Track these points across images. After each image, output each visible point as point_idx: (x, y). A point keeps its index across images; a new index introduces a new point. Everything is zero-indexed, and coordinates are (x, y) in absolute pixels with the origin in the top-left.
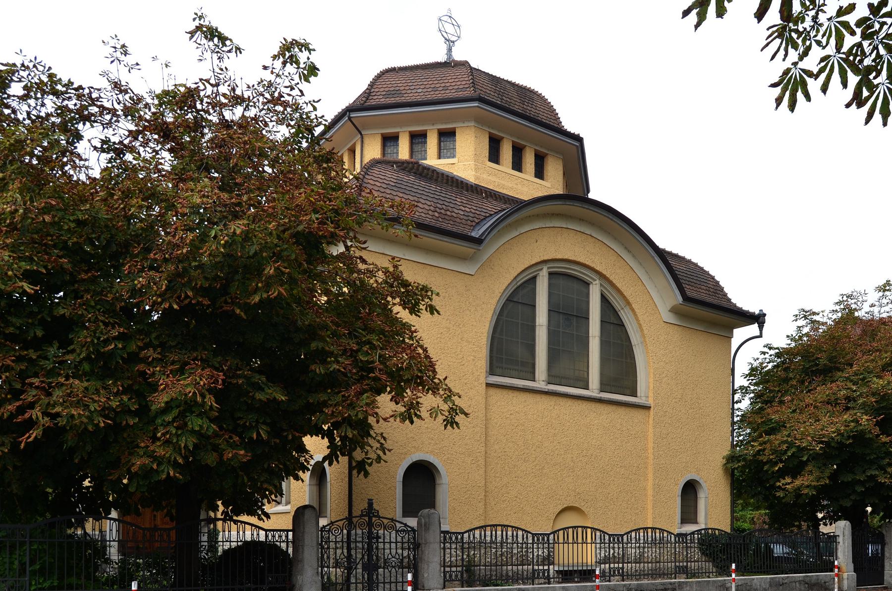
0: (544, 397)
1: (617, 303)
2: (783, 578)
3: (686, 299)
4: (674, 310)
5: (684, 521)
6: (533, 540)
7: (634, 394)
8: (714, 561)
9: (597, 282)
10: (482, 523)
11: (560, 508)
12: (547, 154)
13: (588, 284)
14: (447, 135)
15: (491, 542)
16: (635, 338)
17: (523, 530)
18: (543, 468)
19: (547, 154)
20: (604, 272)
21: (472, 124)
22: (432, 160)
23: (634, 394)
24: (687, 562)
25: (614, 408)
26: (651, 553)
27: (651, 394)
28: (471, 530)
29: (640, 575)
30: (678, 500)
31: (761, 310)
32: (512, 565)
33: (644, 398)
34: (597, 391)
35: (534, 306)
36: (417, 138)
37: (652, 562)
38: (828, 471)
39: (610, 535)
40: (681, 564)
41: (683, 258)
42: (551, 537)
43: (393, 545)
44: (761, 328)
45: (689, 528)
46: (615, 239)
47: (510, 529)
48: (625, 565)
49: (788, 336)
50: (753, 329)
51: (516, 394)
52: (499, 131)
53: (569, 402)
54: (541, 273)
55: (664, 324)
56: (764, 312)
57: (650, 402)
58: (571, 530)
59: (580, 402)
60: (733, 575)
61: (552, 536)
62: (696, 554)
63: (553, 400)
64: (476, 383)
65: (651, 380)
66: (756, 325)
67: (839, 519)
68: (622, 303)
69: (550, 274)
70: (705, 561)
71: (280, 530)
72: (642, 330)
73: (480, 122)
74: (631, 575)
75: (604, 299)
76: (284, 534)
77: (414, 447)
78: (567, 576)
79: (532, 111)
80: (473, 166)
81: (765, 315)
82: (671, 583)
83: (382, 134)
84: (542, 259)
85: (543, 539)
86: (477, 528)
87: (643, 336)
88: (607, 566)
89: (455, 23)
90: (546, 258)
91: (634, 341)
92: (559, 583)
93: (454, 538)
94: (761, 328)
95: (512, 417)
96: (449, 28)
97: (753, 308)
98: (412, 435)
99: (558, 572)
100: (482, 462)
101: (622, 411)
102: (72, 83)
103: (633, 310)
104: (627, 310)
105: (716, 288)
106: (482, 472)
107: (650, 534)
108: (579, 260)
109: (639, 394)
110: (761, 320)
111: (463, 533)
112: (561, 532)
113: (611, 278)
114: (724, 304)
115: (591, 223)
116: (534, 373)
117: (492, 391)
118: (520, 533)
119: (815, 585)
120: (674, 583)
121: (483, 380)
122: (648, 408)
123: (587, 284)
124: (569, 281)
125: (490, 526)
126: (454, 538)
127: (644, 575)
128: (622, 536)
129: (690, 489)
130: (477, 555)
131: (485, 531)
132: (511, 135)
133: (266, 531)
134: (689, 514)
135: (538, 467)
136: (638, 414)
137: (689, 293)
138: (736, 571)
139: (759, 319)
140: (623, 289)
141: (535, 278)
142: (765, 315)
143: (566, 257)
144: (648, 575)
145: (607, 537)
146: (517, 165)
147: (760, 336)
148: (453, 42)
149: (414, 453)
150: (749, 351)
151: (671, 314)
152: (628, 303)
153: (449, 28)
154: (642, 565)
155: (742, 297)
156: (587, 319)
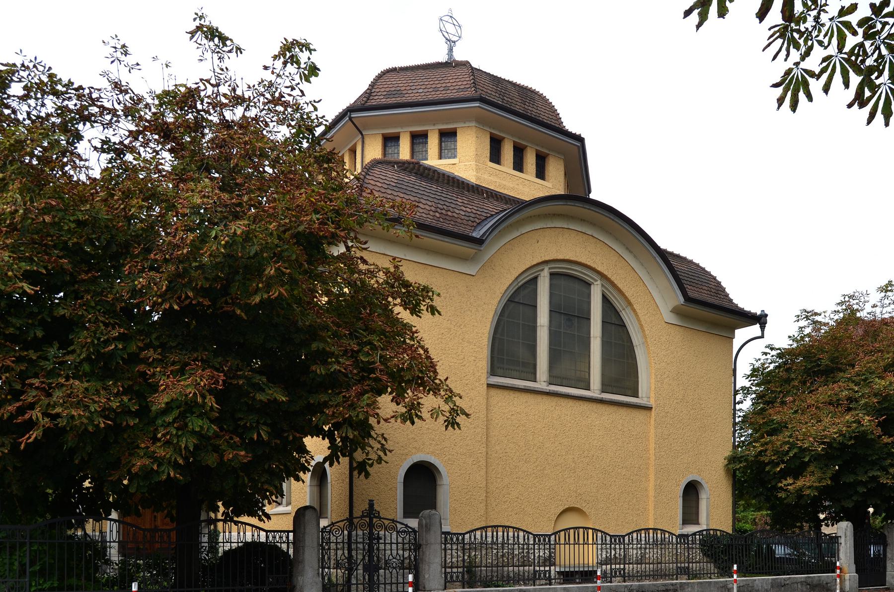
0: (545, 398)
1: (618, 304)
3: (688, 299)
4: (676, 311)
5: (686, 521)
6: (534, 540)
7: (636, 395)
9: (599, 282)
10: (483, 524)
11: (562, 509)
15: (493, 543)
16: (636, 339)
17: (524, 531)
18: (544, 469)
20: (606, 273)
21: (474, 124)
22: (433, 160)
23: (636, 395)
24: (689, 563)
26: (652, 554)
27: (652, 395)
28: (472, 531)
29: (641, 576)
30: (680, 501)
31: (763, 311)
32: (513, 566)
33: (645, 399)
34: (598, 392)
35: (535, 307)
36: (418, 138)
37: (653, 563)
39: (611, 536)
40: (683, 565)
41: (685, 259)
42: (553, 537)
43: (394, 546)
44: (763, 328)
45: (691, 529)
46: (617, 239)
47: (511, 530)
48: (627, 566)
49: (790, 337)
50: (755, 330)
51: (517, 394)
52: (500, 131)
53: (571, 403)
54: (542, 274)
55: (665, 325)
56: (766, 312)
57: (652, 403)
58: (572, 531)
59: (581, 403)
60: (735, 576)
61: (553, 537)
62: (698, 555)
63: (554, 401)
64: (477, 384)
65: (653, 381)
66: (758, 325)
67: (841, 520)
69: (551, 274)
70: (707, 562)
71: (281, 531)
72: (643, 331)
73: (481, 122)
74: (633, 576)
75: (605, 299)
76: (284, 535)
77: (415, 448)
78: (568, 576)
79: (533, 111)
80: (474, 167)
81: (766, 315)
84: (544, 259)
85: (544, 540)
86: (478, 529)
87: (645, 336)
88: (609, 566)
89: (455, 23)
90: (547, 258)
91: (635, 341)
92: (560, 584)
93: (455, 539)
94: (763, 328)
95: (513, 417)
96: (450, 29)
97: (754, 308)
98: (413, 436)
99: (559, 573)
100: (483, 462)
101: (623, 411)
102: (73, 84)
103: (634, 311)
104: (628, 310)
105: (718, 289)
107: (651, 535)
108: (580, 260)
109: (640, 395)
110: (762, 320)
111: (464, 534)
112: (562, 533)
113: (613, 279)
114: (726, 304)
115: (593, 224)
116: (535, 374)
117: (493, 392)
118: (521, 534)
119: (816, 586)
120: (676, 584)
121: (484, 381)
122: (649, 409)
123: (589, 285)
124: (570, 281)
125: (491, 527)
126: (455, 539)
127: (646, 576)
128: (624, 537)
129: (692, 490)
130: (478, 556)
131: (486, 532)
132: (513, 135)
133: (267, 531)
134: (690, 515)
136: (639, 415)
137: (691, 294)
138: (737, 572)
139: (760, 320)
140: (624, 289)
141: (536, 278)
142: (766, 315)
143: (567, 258)
144: (649, 576)
145: (608, 538)
146: (519, 165)
147: (762, 337)
148: (454, 42)
149: (415, 453)
150: (751, 351)
151: (672, 315)
152: (630, 304)
153: (450, 29)
154: (643, 566)
155: (743, 298)
156: (589, 319)
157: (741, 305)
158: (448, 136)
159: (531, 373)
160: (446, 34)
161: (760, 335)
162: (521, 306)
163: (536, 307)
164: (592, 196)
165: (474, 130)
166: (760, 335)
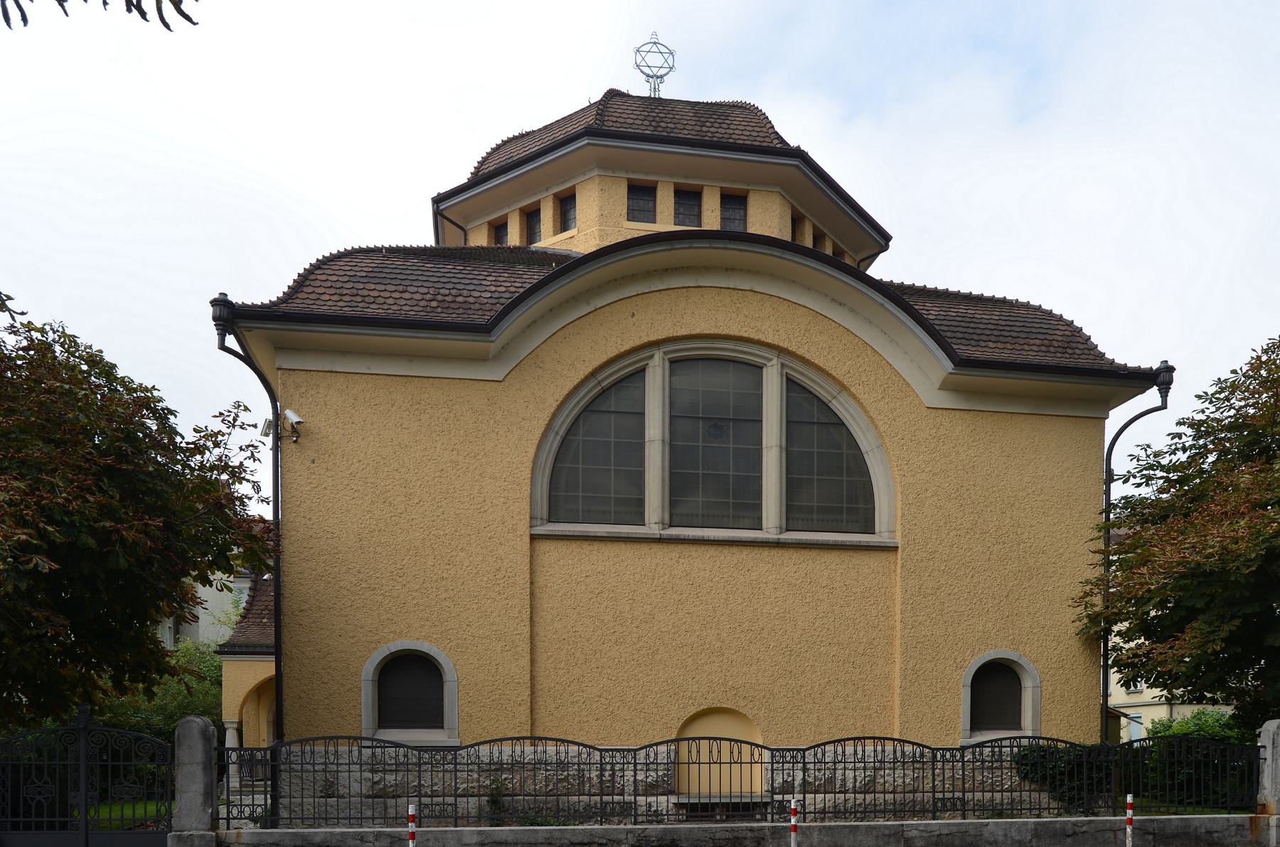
0: (656, 548)
2: (1075, 824)
3: (961, 363)
4: (946, 386)
7: (870, 530)
8: (1052, 789)
9: (775, 361)
12: (748, 191)
13: (760, 368)
16: (865, 441)
19: (748, 191)
22: (548, 241)
25: (814, 553)
26: (900, 777)
27: (899, 527)
29: (864, 812)
30: (966, 695)
33: (886, 535)
34: (774, 531)
36: (531, 217)
37: (894, 792)
38: (1226, 628)
46: (808, 288)
47: (725, 745)
49: (1199, 397)
50: (1152, 396)
52: (686, 177)
53: (712, 551)
54: (651, 363)
56: (1170, 363)
57: (898, 540)
59: (735, 550)
60: (1130, 812)
62: (1010, 778)
65: (899, 504)
68: (833, 389)
69: (672, 362)
70: (1030, 791)
73: (607, 166)
75: (792, 385)
76: (958, 754)
77: (394, 632)
79: (740, 137)
80: (596, 233)
81: (1172, 369)
82: (752, 830)
84: (645, 340)
89: (663, 49)
90: (652, 338)
94: (1164, 393)
97: (1150, 361)
99: (679, 806)
103: (854, 396)
104: (843, 398)
105: (1072, 336)
106: (525, 661)
109: (877, 529)
110: (1161, 378)
113: (800, 352)
114: (1083, 362)
116: (642, 514)
117: (544, 546)
119: (1175, 836)
120: (762, 829)
121: (524, 530)
132: (671, 175)
133: (601, 751)
135: (644, 651)
137: (963, 350)
138: (1132, 806)
139: (1161, 378)
141: (642, 371)
142: (1172, 369)
143: (698, 331)
150: (1142, 436)
151: (943, 394)
152: (844, 388)
155: (1122, 346)
157: (1120, 360)
158: (566, 203)
159: (750, 512)
160: (647, 70)
161: (1159, 403)
162: (613, 416)
163: (642, 414)
164: (751, 230)
165: (597, 180)
166: (1159, 403)
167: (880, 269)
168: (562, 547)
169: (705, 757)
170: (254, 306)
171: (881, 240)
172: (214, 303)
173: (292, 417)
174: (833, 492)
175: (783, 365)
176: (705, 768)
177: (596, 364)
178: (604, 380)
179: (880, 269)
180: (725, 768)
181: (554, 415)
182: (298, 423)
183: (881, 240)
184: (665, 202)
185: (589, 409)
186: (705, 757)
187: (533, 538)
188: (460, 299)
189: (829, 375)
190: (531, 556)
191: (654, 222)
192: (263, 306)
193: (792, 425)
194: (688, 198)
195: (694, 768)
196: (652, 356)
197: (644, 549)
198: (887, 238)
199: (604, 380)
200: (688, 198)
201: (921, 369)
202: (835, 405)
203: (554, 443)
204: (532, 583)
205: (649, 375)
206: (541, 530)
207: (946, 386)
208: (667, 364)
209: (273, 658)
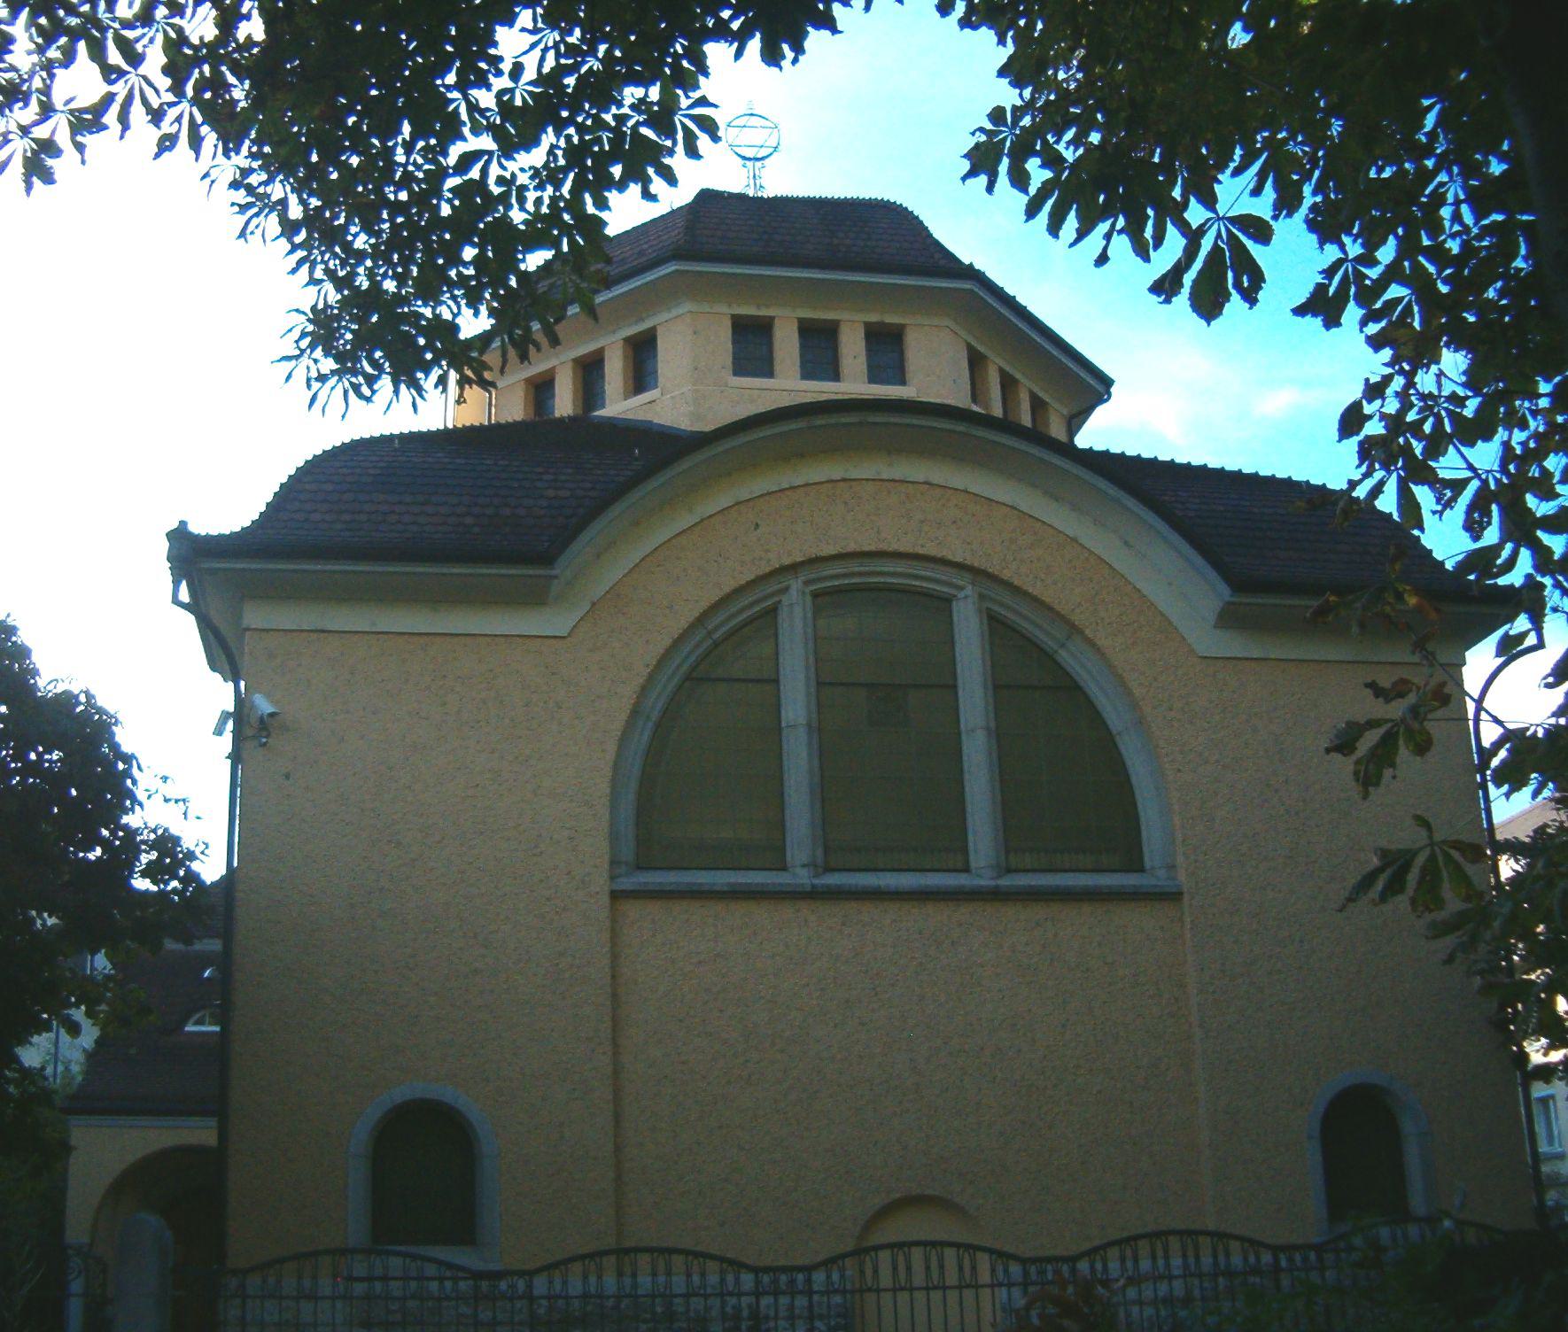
3: (1239, 583)
9: (969, 590)
14: (642, 351)
22: (617, 405)
23: (1134, 863)
33: (1162, 873)
54: (785, 599)
69: (816, 595)
75: (996, 625)
83: (801, 322)
103: (1090, 642)
116: (964, 850)
121: (601, 883)
122: (1174, 896)
123: (947, 601)
124: (883, 599)
125: (924, 1244)
136: (1139, 921)
141: (773, 611)
152: (1074, 629)
163: (954, 687)
167: (1100, 432)
168: (655, 908)
169: (886, 1280)
170: (221, 536)
171: (1091, 387)
172: (171, 536)
173: (264, 705)
174: (1078, 810)
175: (982, 597)
176: (887, 1298)
177: (704, 605)
178: (716, 628)
179: (1100, 432)
180: (920, 1296)
181: (644, 690)
182: (272, 715)
183: (1091, 387)
184: (852, 347)
185: (694, 679)
186: (886, 1280)
187: (616, 896)
188: (507, 511)
189: (1026, 594)
190: (613, 930)
191: (836, 377)
192: (234, 535)
193: (1000, 688)
194: (820, 347)
195: (871, 1298)
196: (787, 589)
197: (787, 910)
198: (1107, 383)
199: (716, 628)
200: (820, 347)
201: (1175, 589)
202: (1064, 656)
203: (643, 737)
204: (613, 977)
205: (783, 614)
206: (627, 883)
207: (1228, 619)
208: (809, 599)
209: (213, 1122)
